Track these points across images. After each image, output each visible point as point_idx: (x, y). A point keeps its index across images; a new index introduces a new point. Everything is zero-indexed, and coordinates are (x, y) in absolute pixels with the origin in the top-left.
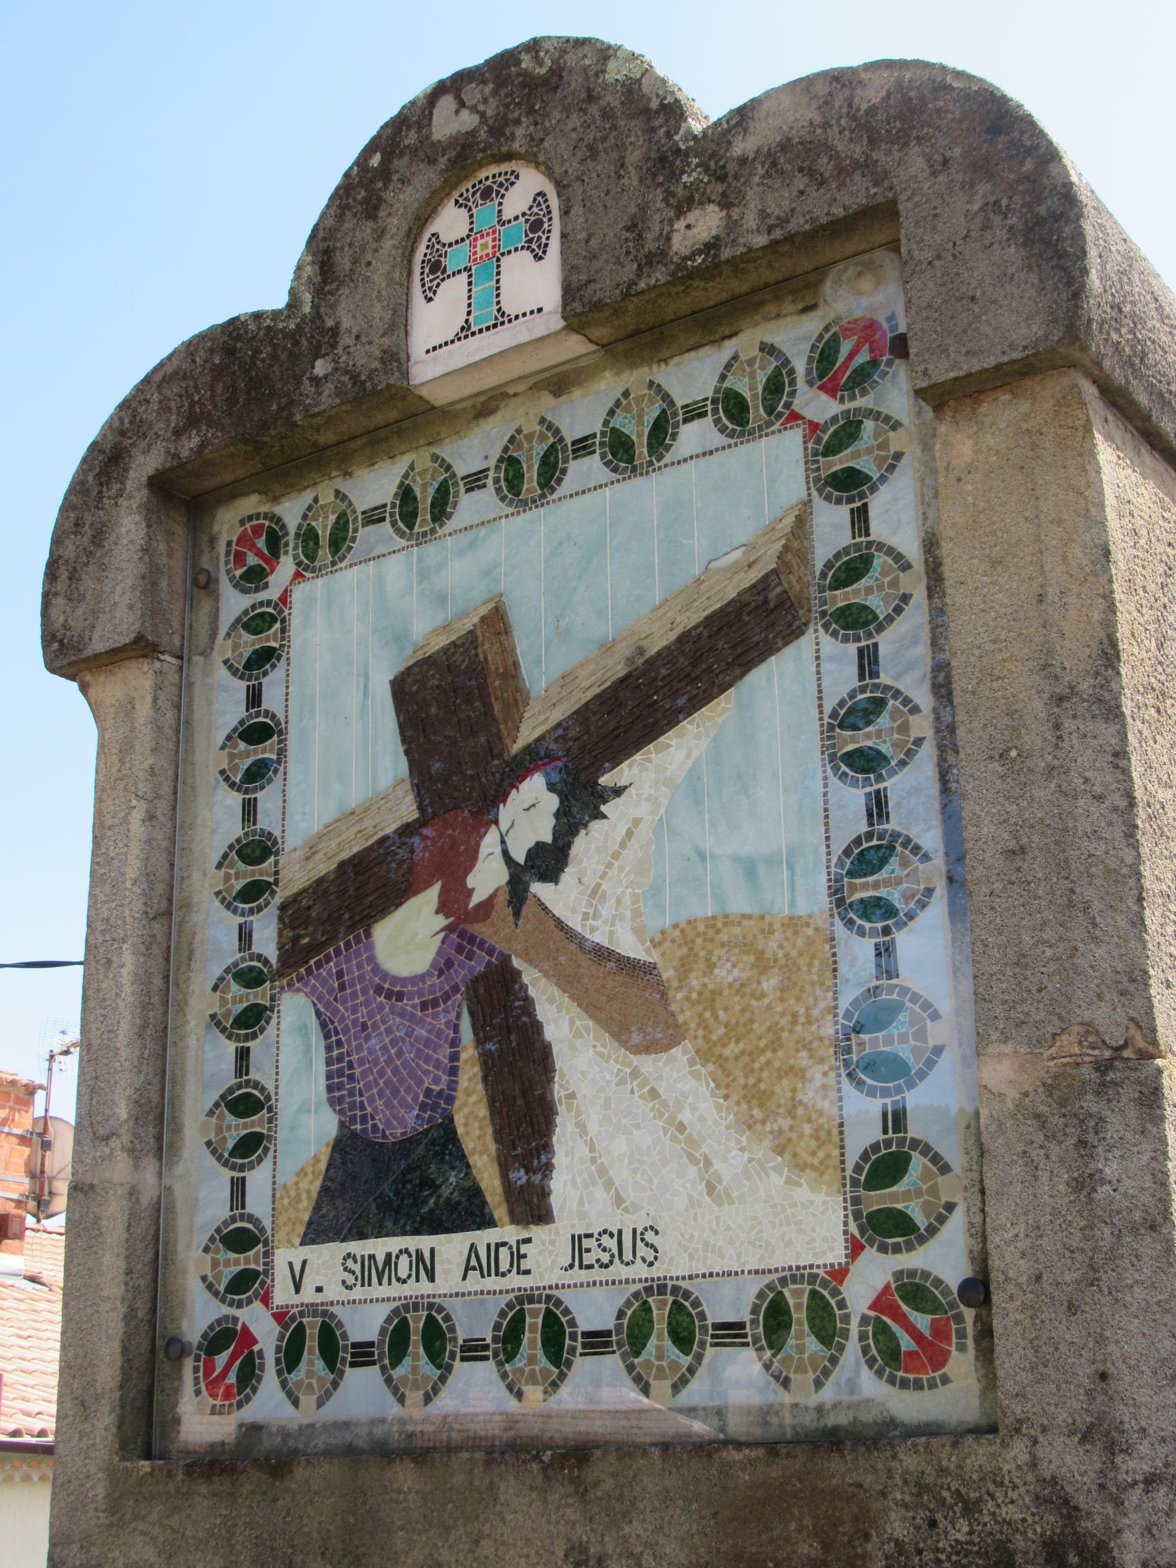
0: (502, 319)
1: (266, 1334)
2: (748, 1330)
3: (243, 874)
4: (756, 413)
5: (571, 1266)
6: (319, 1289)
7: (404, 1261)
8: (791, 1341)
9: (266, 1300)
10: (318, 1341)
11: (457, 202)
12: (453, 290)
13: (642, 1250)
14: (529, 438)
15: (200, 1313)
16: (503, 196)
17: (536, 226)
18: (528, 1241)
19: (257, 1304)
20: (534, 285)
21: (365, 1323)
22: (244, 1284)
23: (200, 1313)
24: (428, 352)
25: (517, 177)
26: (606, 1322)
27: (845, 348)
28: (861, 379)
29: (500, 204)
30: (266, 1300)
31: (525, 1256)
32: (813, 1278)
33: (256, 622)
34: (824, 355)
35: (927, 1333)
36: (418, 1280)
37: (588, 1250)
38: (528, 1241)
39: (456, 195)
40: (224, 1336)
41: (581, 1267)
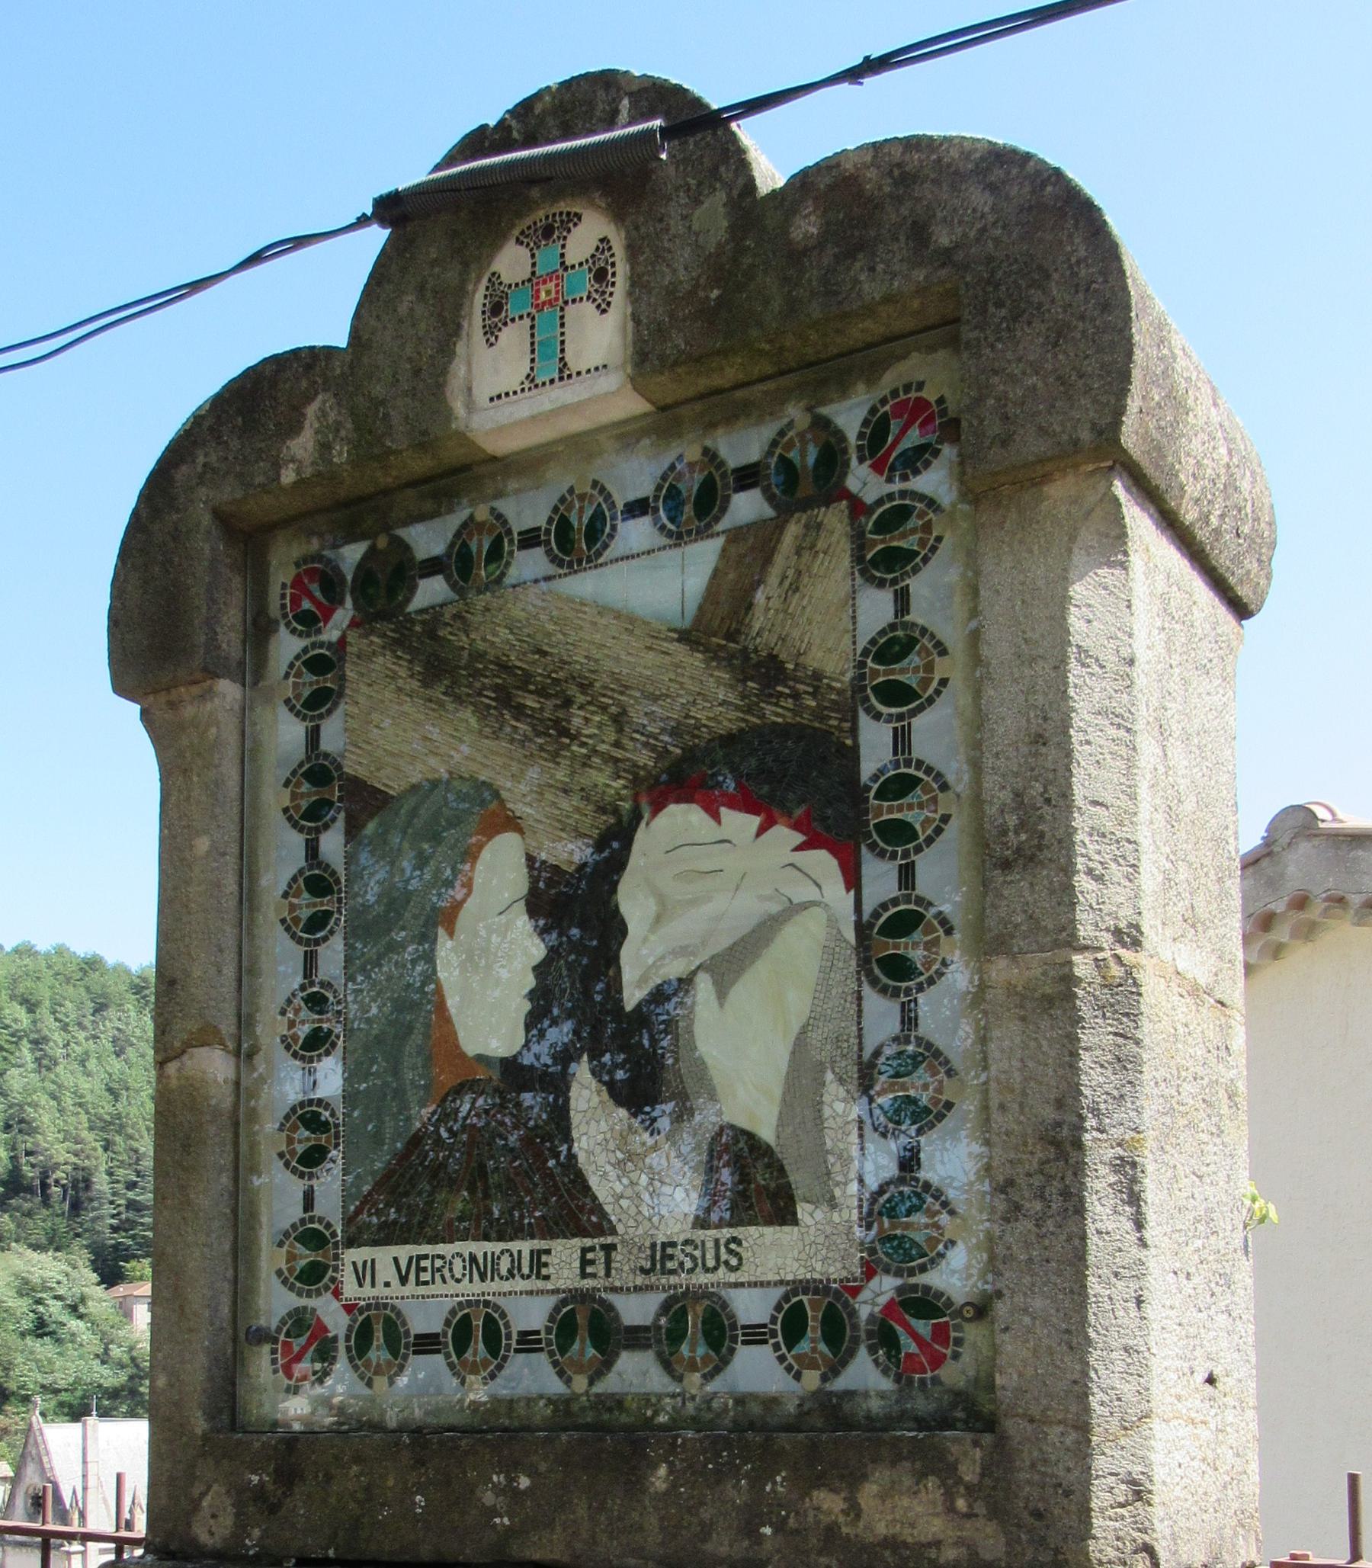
0: (564, 373)
1: (336, 1321)
2: (543, 1336)
3: (306, 905)
4: (806, 488)
5: (653, 1269)
6: (387, 1284)
7: (458, 1265)
8: (576, 1346)
9: (337, 1294)
10: (379, 1334)
11: (518, 239)
12: (514, 337)
13: (697, 1253)
14: (582, 497)
15: (276, 1302)
16: (565, 238)
17: (601, 276)
18: (548, 1252)
19: (328, 1296)
20: (599, 335)
21: (426, 1315)
22: (313, 1277)
23: (276, 1302)
24: (492, 399)
25: (580, 219)
26: (436, 1326)
27: (895, 426)
28: (916, 460)
29: (563, 246)
30: (337, 1294)
31: (546, 1265)
32: (827, 1290)
33: (317, 664)
34: (876, 433)
35: (928, 1338)
36: (471, 1281)
37: (592, 1262)
38: (548, 1252)
39: (516, 232)
40: (299, 1321)
41: (538, 1277)
